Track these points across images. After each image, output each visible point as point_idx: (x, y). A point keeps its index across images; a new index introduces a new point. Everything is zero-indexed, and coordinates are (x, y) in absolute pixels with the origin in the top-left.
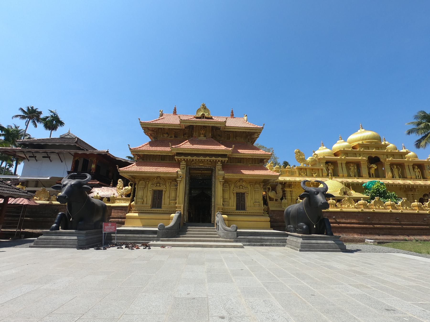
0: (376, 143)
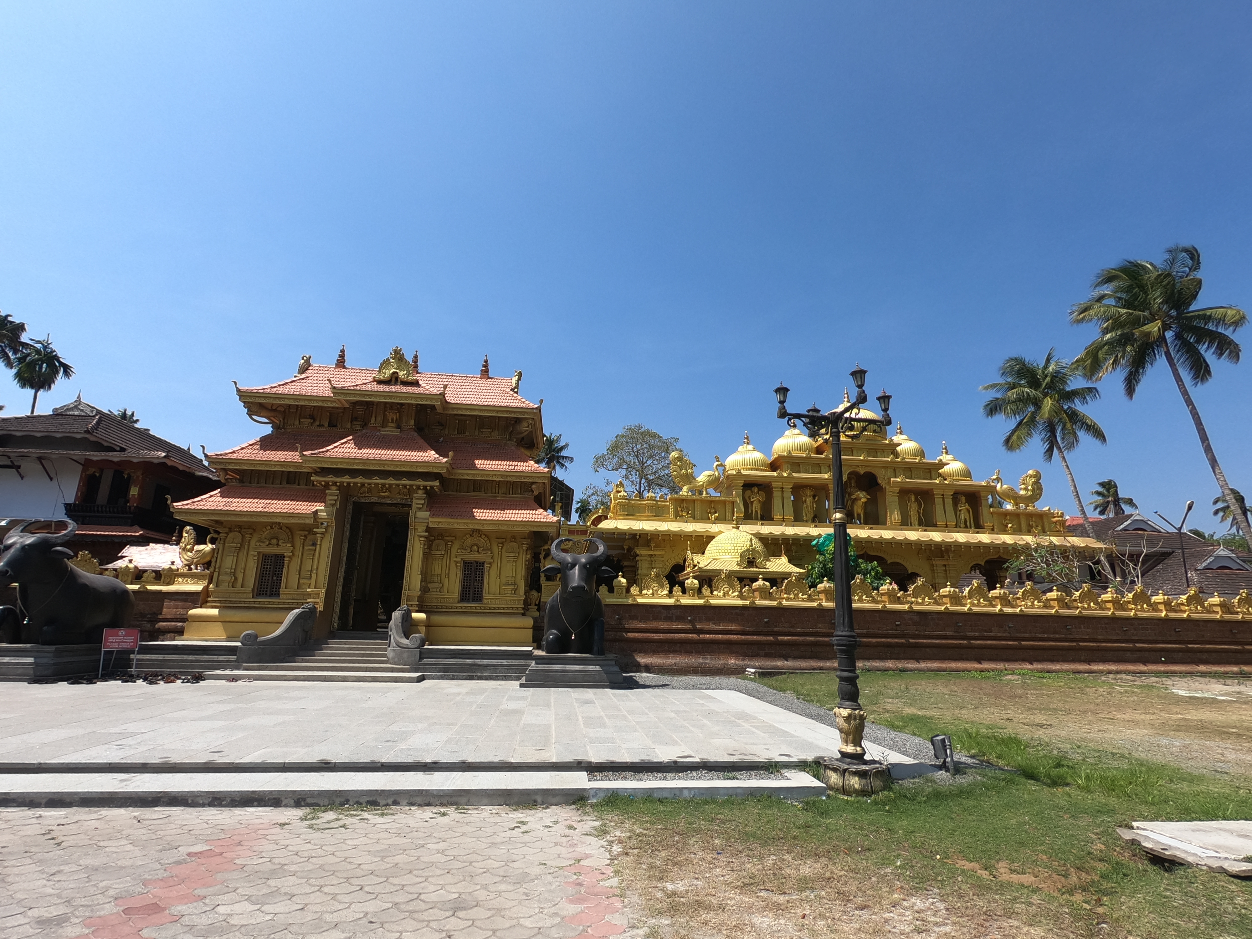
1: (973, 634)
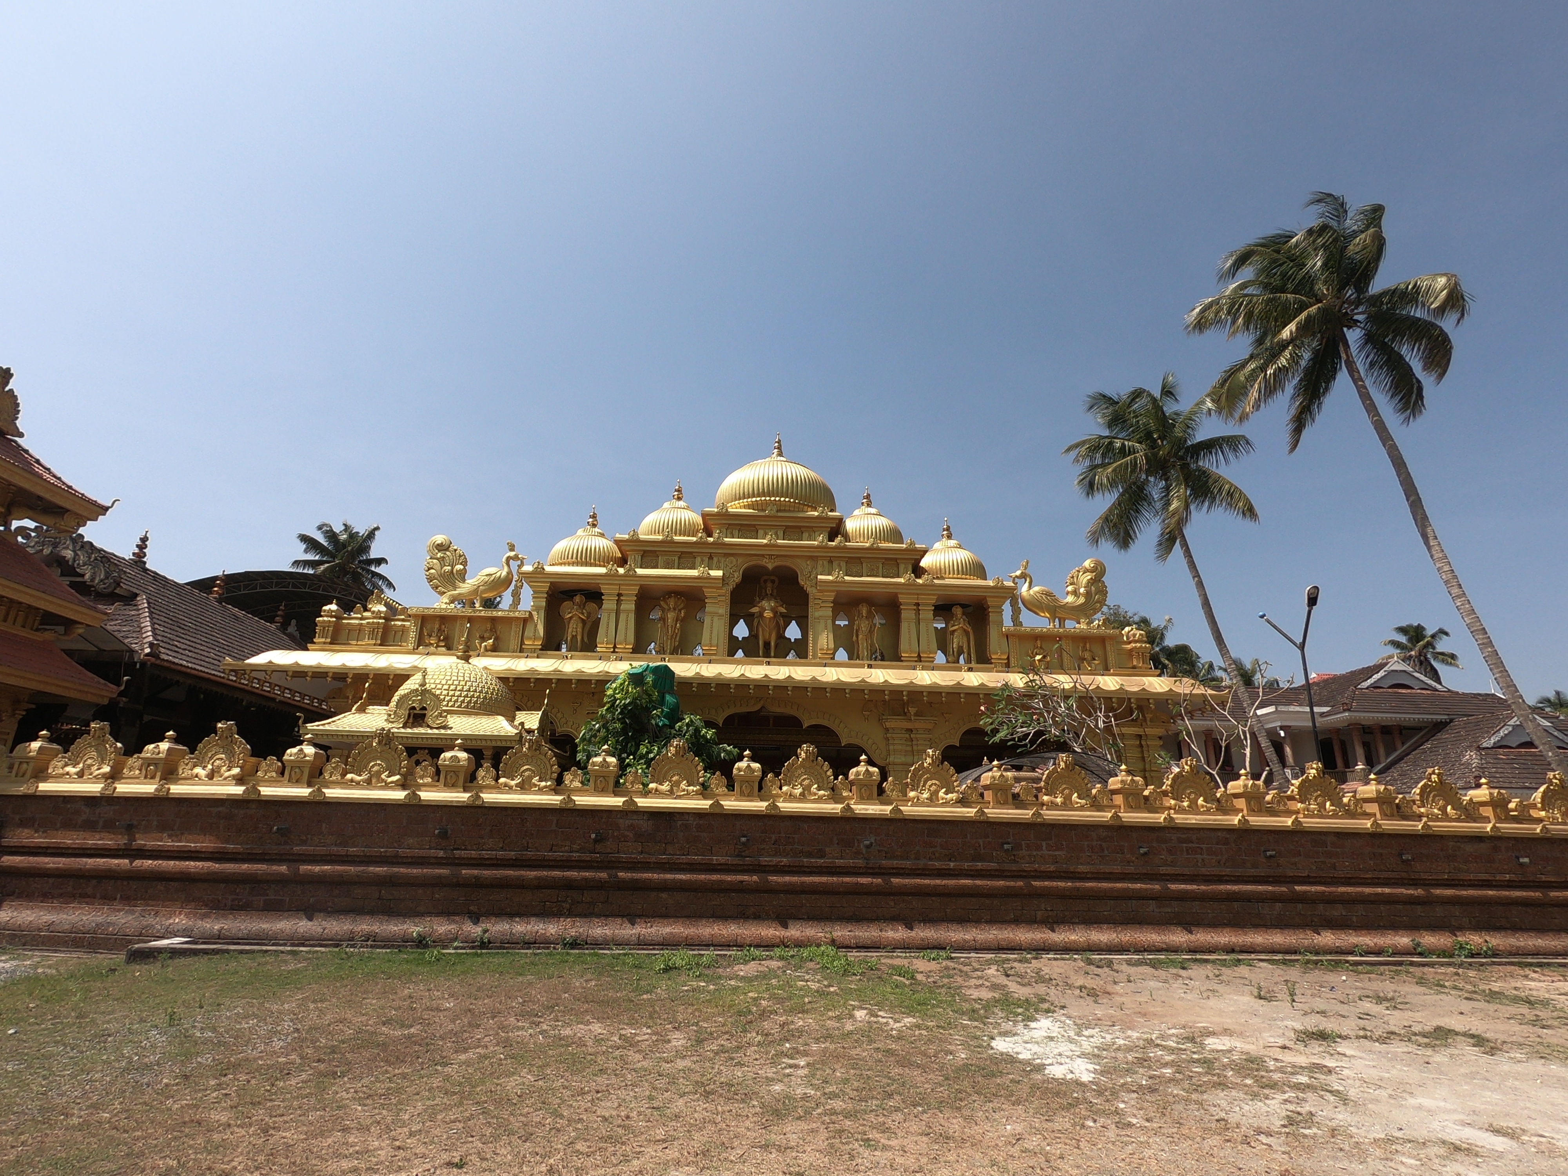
0: (801, 508)
1: (775, 860)
